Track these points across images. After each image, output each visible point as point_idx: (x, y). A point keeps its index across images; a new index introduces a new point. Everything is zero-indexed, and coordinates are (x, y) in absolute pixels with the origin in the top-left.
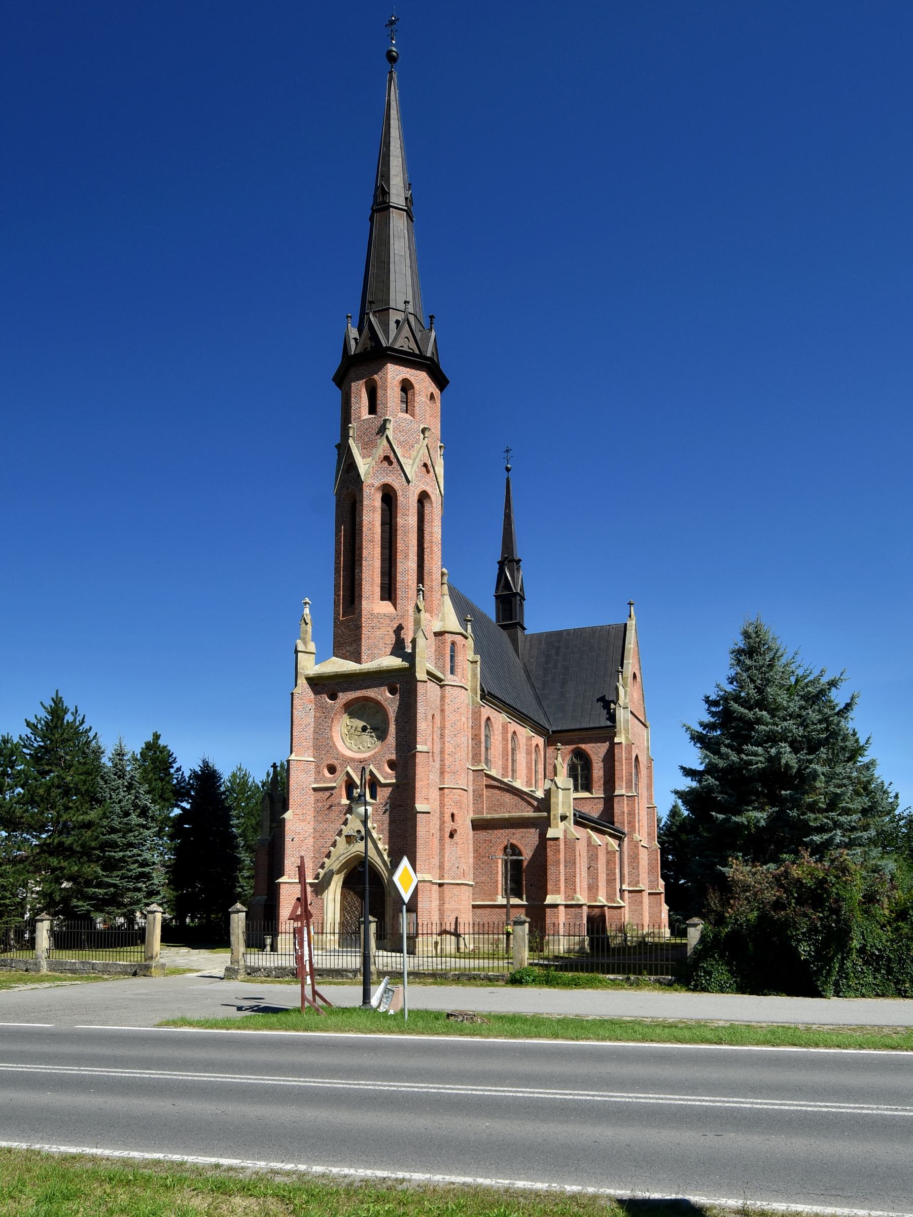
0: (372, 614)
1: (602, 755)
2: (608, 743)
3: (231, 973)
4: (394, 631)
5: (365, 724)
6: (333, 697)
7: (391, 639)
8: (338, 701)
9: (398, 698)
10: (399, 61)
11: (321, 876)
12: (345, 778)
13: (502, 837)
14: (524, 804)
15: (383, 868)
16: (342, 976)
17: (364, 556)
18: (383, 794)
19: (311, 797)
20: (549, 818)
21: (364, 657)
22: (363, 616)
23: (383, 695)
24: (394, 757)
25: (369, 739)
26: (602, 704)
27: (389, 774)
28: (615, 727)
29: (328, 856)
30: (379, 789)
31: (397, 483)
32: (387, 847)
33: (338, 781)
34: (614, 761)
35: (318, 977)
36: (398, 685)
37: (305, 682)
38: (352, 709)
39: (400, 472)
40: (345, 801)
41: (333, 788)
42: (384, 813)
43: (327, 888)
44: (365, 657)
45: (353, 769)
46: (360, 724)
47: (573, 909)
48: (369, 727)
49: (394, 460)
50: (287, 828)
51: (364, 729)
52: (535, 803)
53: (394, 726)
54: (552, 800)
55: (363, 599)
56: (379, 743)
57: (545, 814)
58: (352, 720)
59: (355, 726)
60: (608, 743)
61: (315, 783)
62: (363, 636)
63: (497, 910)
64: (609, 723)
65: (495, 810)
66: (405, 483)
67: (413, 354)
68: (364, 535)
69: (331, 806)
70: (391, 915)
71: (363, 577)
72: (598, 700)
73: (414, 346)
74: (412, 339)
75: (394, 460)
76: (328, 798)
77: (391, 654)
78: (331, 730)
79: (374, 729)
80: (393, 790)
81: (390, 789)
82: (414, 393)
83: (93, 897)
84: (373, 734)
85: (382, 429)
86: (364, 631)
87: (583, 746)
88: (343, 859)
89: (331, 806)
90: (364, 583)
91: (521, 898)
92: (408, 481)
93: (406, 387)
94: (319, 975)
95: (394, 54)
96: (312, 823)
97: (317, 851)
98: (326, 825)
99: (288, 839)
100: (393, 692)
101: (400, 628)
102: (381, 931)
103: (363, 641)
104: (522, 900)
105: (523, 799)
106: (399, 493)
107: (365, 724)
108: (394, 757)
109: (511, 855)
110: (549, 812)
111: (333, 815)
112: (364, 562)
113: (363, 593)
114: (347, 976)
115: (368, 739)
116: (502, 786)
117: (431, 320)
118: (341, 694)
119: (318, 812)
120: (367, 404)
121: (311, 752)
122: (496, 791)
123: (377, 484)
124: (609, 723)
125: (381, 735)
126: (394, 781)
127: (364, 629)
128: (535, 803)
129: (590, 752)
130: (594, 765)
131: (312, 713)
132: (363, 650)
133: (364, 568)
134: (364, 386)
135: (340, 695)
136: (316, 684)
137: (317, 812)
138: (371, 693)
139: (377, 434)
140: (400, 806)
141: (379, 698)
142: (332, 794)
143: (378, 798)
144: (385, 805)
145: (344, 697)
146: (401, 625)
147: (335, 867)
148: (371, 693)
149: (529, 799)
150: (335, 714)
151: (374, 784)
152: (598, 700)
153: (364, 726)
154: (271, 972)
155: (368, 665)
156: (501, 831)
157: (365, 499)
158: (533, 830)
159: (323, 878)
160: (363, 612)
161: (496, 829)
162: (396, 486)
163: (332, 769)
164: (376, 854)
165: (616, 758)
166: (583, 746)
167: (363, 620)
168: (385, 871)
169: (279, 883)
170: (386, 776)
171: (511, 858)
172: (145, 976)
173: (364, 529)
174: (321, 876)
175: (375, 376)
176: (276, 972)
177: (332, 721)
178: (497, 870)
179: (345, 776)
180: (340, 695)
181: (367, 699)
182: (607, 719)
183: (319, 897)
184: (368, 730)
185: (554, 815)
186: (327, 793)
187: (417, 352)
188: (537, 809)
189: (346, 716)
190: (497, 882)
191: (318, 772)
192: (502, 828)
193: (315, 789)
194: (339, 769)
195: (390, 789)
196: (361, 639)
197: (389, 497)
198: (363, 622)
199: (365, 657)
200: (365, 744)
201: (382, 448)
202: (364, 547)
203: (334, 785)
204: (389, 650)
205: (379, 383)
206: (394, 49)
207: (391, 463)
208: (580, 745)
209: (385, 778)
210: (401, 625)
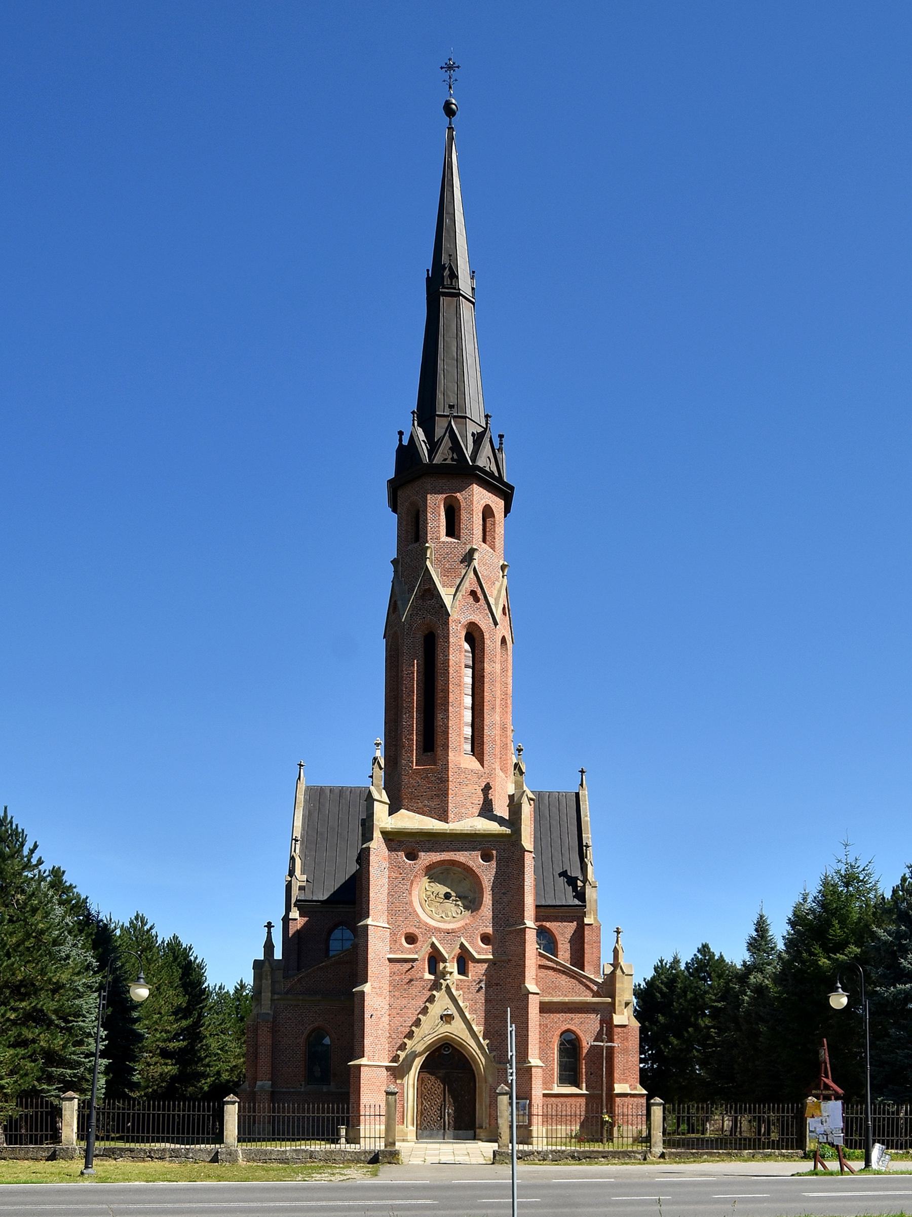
0: (459, 768)
1: (569, 936)
2: (575, 923)
3: (497, 1157)
4: (482, 790)
5: (449, 890)
6: (412, 856)
7: (479, 799)
8: (419, 861)
9: (495, 866)
10: (458, 113)
11: (401, 1059)
12: (429, 949)
13: (563, 1022)
14: (583, 988)
15: (478, 1051)
16: (630, 1157)
17: (450, 701)
18: (477, 971)
19: (386, 969)
20: (613, 1004)
21: (451, 815)
22: (450, 769)
23: (472, 859)
24: (490, 930)
25: (454, 908)
26: (566, 880)
27: (483, 949)
28: (585, 906)
29: (410, 1035)
30: (471, 965)
31: (485, 624)
32: (482, 1028)
33: (421, 952)
34: (583, 943)
35: (603, 1159)
36: (494, 852)
37: (381, 836)
38: (435, 873)
39: (487, 611)
40: (428, 976)
41: (414, 960)
42: (478, 991)
43: (408, 1073)
44: (453, 816)
45: (439, 941)
46: (443, 889)
47: (635, 1099)
48: (453, 894)
49: (481, 597)
50: (366, 1003)
51: (447, 896)
52: (595, 988)
53: (490, 897)
54: (617, 985)
55: (450, 750)
56: (467, 913)
57: (609, 1000)
58: (432, 884)
59: (436, 892)
60: (575, 923)
61: (390, 952)
62: (450, 791)
63: (553, 1099)
64: (577, 902)
65: (549, 993)
66: (492, 625)
67: (491, 474)
68: (451, 677)
69: (411, 980)
70: (488, 1103)
71: (450, 725)
72: (560, 875)
73: (494, 469)
74: (493, 460)
75: (481, 597)
76: (407, 971)
77: (478, 816)
78: (410, 894)
79: (460, 897)
80: (488, 967)
81: (485, 966)
82: (494, 522)
83: (61, 1079)
84: (459, 903)
85: (468, 558)
86: (451, 786)
87: (548, 924)
88: (428, 1040)
89: (411, 980)
90: (450, 732)
91: (578, 1086)
92: (496, 624)
93: (488, 512)
94: (603, 1157)
95: (454, 106)
96: (387, 998)
97: (393, 1030)
98: (405, 1002)
99: (367, 1016)
100: (486, 857)
101: (487, 789)
102: (83, 1131)
103: (450, 796)
104: (581, 1089)
105: (581, 982)
106: (486, 636)
107: (449, 890)
108: (490, 930)
109: (607, 1042)
110: (613, 997)
111: (414, 991)
112: (450, 708)
113: (450, 743)
114: (635, 1157)
115: (452, 908)
116: (558, 967)
117: (501, 440)
118: (423, 854)
119: (394, 986)
120: (445, 523)
121: (385, 917)
122: (550, 972)
123: (464, 621)
124: (577, 902)
125: (472, 903)
126: (491, 957)
127: (450, 783)
128: (595, 988)
129: (555, 932)
130: (560, 946)
131: (386, 872)
132: (450, 808)
133: (450, 715)
134: (443, 502)
135: (422, 854)
136: (390, 840)
137: (394, 986)
138: (461, 857)
139: (462, 562)
140: (497, 985)
141: (471, 864)
142: (413, 967)
143: (470, 975)
144: (479, 983)
145: (427, 858)
146: (488, 784)
147: (420, 1048)
148: (461, 857)
149: (588, 983)
150: (415, 876)
151: (464, 960)
152: (560, 875)
153: (447, 893)
154: (547, 1155)
155: (455, 826)
156: (558, 1015)
157: (451, 636)
158: (593, 1016)
159: (404, 1060)
160: (450, 765)
161: (553, 1013)
162: (483, 627)
163: (411, 939)
164: (469, 1036)
165: (586, 941)
166: (548, 924)
167: (450, 773)
168: (480, 1055)
169: (359, 1066)
170: (483, 952)
171: (606, 1044)
172: (390, 1163)
173: (451, 671)
174: (401, 1059)
175: (458, 494)
176: (552, 1155)
177: (412, 884)
178: (553, 1057)
179: (429, 948)
180: (422, 854)
181: (453, 863)
182: (574, 897)
183: (399, 1081)
184: (453, 898)
185: (620, 1001)
186: (407, 966)
187: (496, 474)
188: (596, 994)
189: (425, 880)
190: (553, 1069)
191: (394, 941)
192: (559, 1013)
193: (390, 960)
194: (420, 938)
195: (485, 966)
196: (447, 794)
197: (474, 636)
198: (450, 776)
199: (453, 816)
200: (450, 914)
201: (470, 583)
202: (450, 690)
203: (416, 956)
204: (476, 811)
205: (463, 504)
206: (454, 101)
207: (477, 600)
208: (544, 923)
209: (479, 953)
210: (488, 784)
